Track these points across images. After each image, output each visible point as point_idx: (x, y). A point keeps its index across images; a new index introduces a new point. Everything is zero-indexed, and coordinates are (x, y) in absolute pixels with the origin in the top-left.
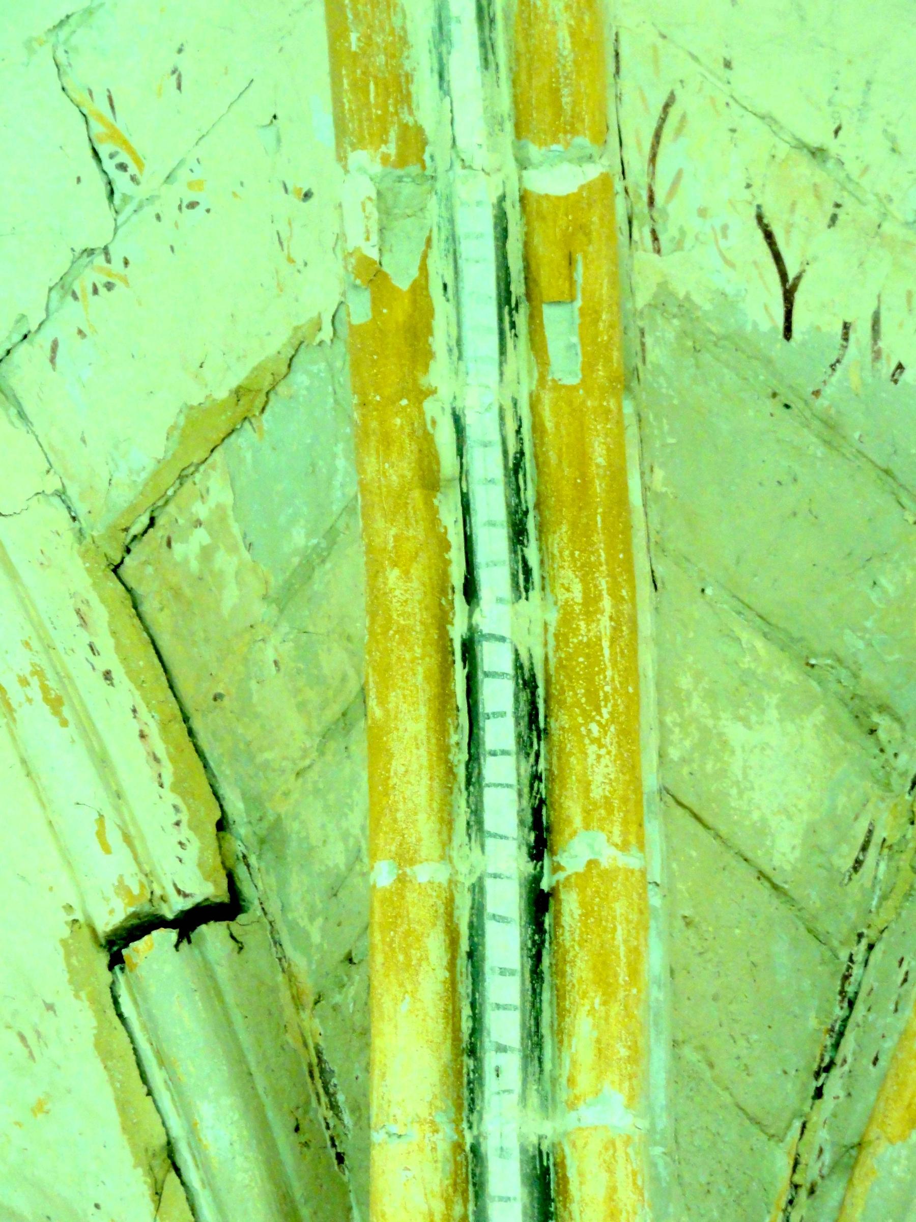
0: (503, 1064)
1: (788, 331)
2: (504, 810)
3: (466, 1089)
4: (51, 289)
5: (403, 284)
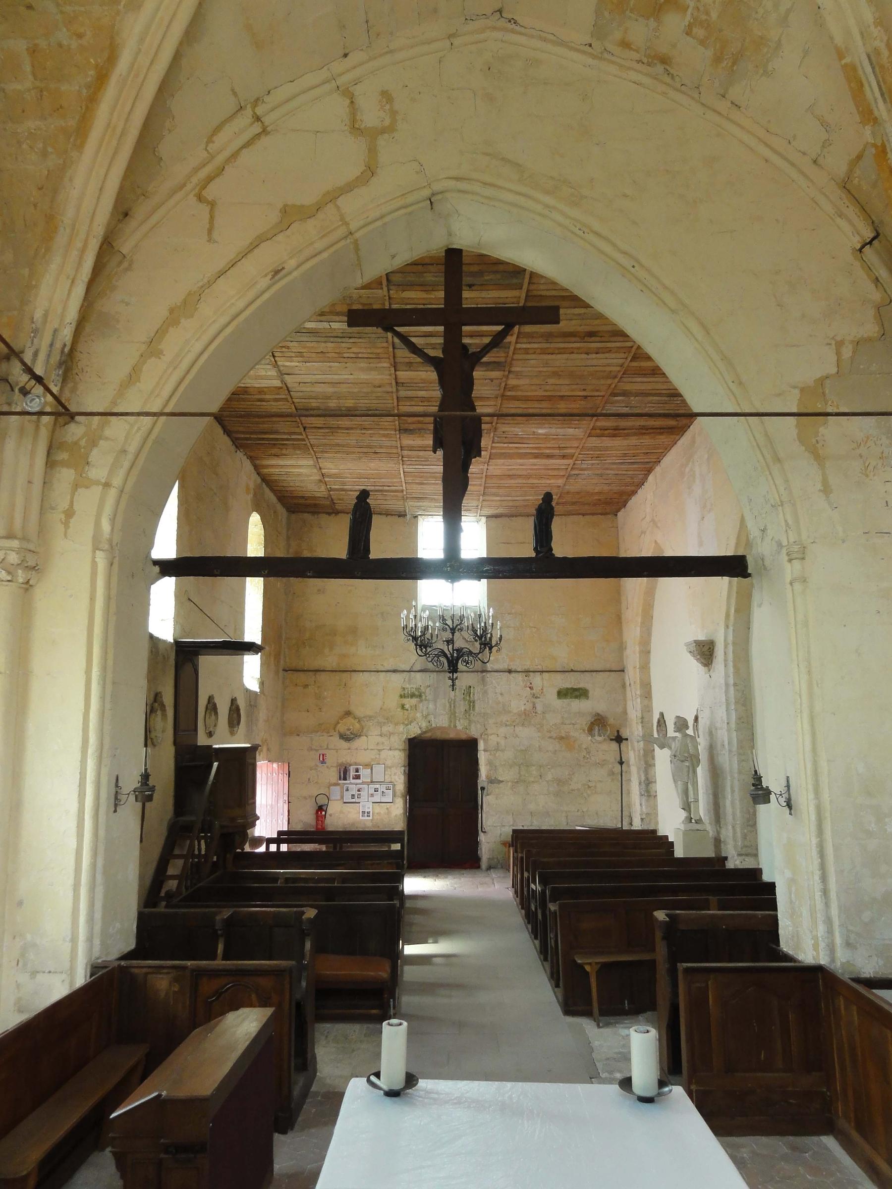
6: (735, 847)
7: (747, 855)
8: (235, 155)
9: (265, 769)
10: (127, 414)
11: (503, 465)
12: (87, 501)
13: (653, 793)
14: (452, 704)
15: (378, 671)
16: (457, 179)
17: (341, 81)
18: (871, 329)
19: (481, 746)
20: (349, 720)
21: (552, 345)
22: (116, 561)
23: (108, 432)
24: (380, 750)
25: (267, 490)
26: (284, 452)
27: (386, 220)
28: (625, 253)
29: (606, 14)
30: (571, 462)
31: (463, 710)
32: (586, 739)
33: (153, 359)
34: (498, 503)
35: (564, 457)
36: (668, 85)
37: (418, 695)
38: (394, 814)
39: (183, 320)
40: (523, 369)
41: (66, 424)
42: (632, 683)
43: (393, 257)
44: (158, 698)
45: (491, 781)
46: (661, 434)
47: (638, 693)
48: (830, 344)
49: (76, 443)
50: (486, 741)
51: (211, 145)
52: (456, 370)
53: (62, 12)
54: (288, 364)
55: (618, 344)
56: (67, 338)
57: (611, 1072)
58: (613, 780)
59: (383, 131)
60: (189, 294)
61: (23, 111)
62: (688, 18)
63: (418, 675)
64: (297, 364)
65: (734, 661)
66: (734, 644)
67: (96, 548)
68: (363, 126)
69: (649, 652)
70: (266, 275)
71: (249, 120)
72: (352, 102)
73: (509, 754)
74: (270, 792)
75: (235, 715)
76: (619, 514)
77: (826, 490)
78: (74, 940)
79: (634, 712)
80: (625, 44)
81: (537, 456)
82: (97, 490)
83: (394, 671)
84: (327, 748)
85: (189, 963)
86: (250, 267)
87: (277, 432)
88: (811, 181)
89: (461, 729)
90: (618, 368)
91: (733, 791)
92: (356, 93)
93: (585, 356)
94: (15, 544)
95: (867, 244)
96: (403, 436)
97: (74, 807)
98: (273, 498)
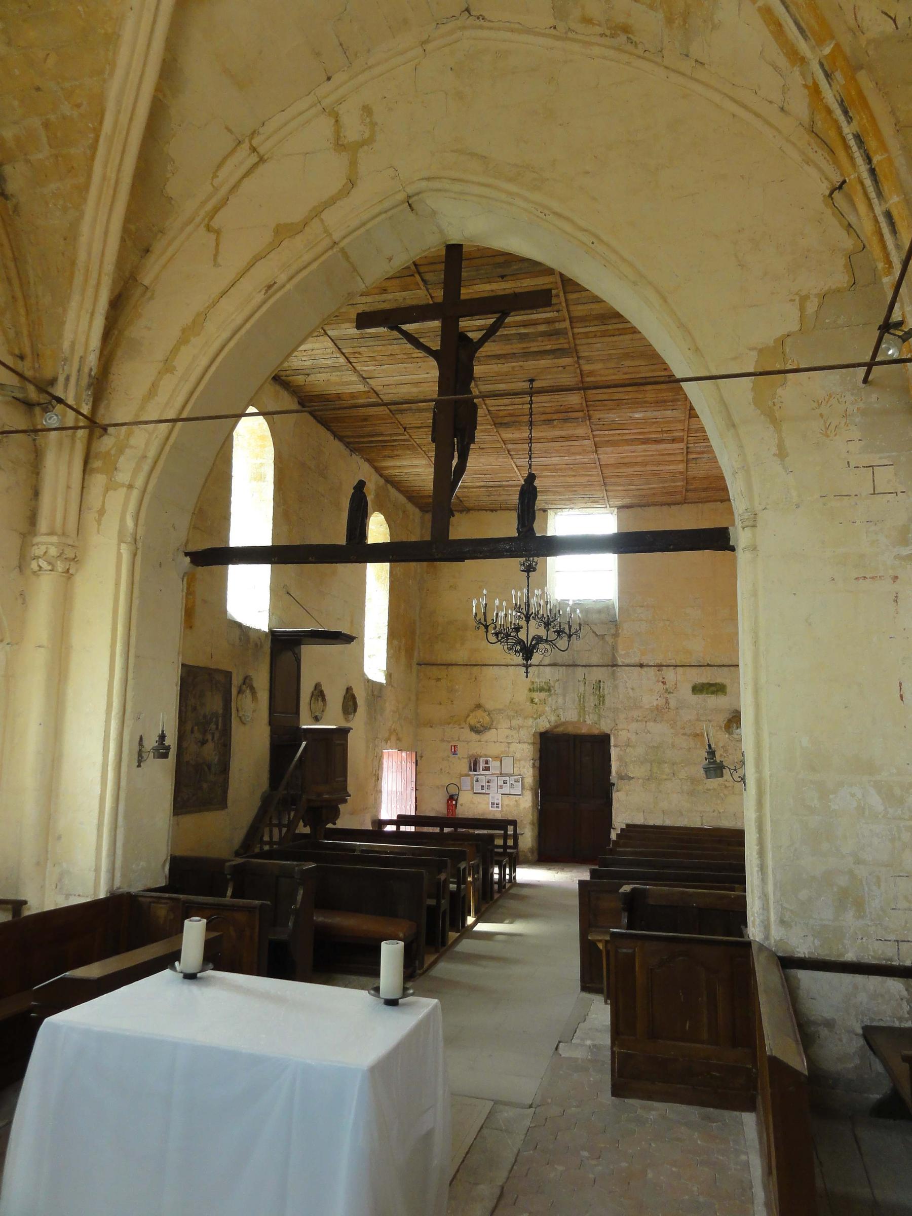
0: (875, 201)
2: (860, 160)
3: (871, 206)
5: (811, 84)
9: (395, 757)
10: (146, 423)
11: (612, 453)
12: (116, 500)
14: (582, 698)
15: (507, 666)
16: (428, 179)
17: (326, 102)
18: (840, 279)
20: (479, 713)
21: (610, 327)
22: (139, 553)
23: (133, 441)
25: (393, 491)
26: (396, 453)
27: (368, 226)
30: (681, 445)
31: (593, 705)
33: (168, 374)
35: (673, 440)
36: (631, 54)
37: (547, 689)
38: (522, 807)
40: (591, 354)
41: (101, 436)
43: (390, 259)
44: (248, 681)
45: (621, 778)
48: (794, 300)
50: (616, 738)
53: (62, 88)
54: (366, 368)
56: (93, 364)
57: (582, 1039)
59: (363, 143)
63: (548, 669)
64: (374, 368)
67: (121, 540)
72: (337, 121)
73: (640, 750)
74: (399, 777)
75: (351, 703)
77: (782, 454)
78: (97, 870)
80: (587, 21)
81: (646, 441)
84: (459, 740)
85: (181, 896)
86: (246, 285)
87: (382, 435)
88: (777, 129)
89: (591, 724)
92: (341, 112)
94: (54, 539)
95: (836, 189)
96: (501, 430)
97: (99, 759)
98: (402, 499)
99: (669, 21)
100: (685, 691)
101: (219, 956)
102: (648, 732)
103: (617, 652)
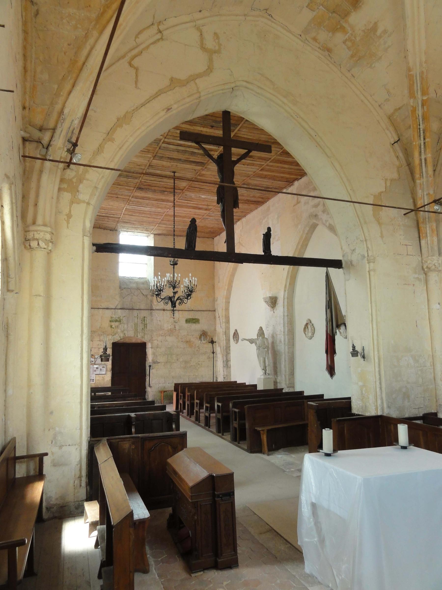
1: (13, 91)
2: (422, 139)
4: (135, 40)
6: (286, 384)
7: (290, 387)
8: (148, 47)
13: (229, 366)
14: (136, 325)
15: (98, 309)
18: (395, 175)
19: (149, 346)
23: (88, 176)
24: (99, 348)
28: (312, 129)
29: (312, 25)
32: (198, 342)
34: (164, 228)
35: (206, 209)
37: (119, 321)
38: (106, 380)
39: (124, 125)
42: (221, 317)
43: (206, 110)
45: (154, 362)
46: (253, 204)
47: (224, 321)
49: (71, 180)
50: (152, 343)
51: (137, 39)
52: (225, 166)
55: (259, 163)
56: (76, 126)
58: (209, 361)
59: (215, 52)
60: (127, 112)
61: (68, 3)
62: (347, 37)
63: (119, 311)
65: (287, 306)
66: (287, 298)
67: (84, 235)
68: (206, 47)
69: (229, 302)
70: (163, 110)
71: (156, 31)
72: (201, 34)
76: (215, 238)
77: (382, 237)
79: (220, 329)
80: (315, 39)
82: (84, 206)
83: (107, 309)
85: (140, 435)
89: (139, 338)
90: (252, 173)
91: (285, 361)
93: (243, 166)
99: (352, 56)
100: (183, 322)
101: (341, 444)
102: (167, 341)
103: (153, 303)
